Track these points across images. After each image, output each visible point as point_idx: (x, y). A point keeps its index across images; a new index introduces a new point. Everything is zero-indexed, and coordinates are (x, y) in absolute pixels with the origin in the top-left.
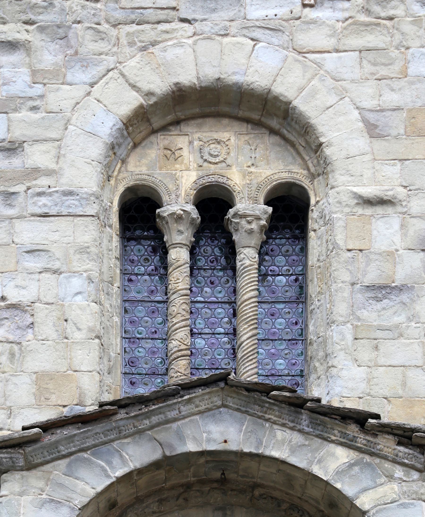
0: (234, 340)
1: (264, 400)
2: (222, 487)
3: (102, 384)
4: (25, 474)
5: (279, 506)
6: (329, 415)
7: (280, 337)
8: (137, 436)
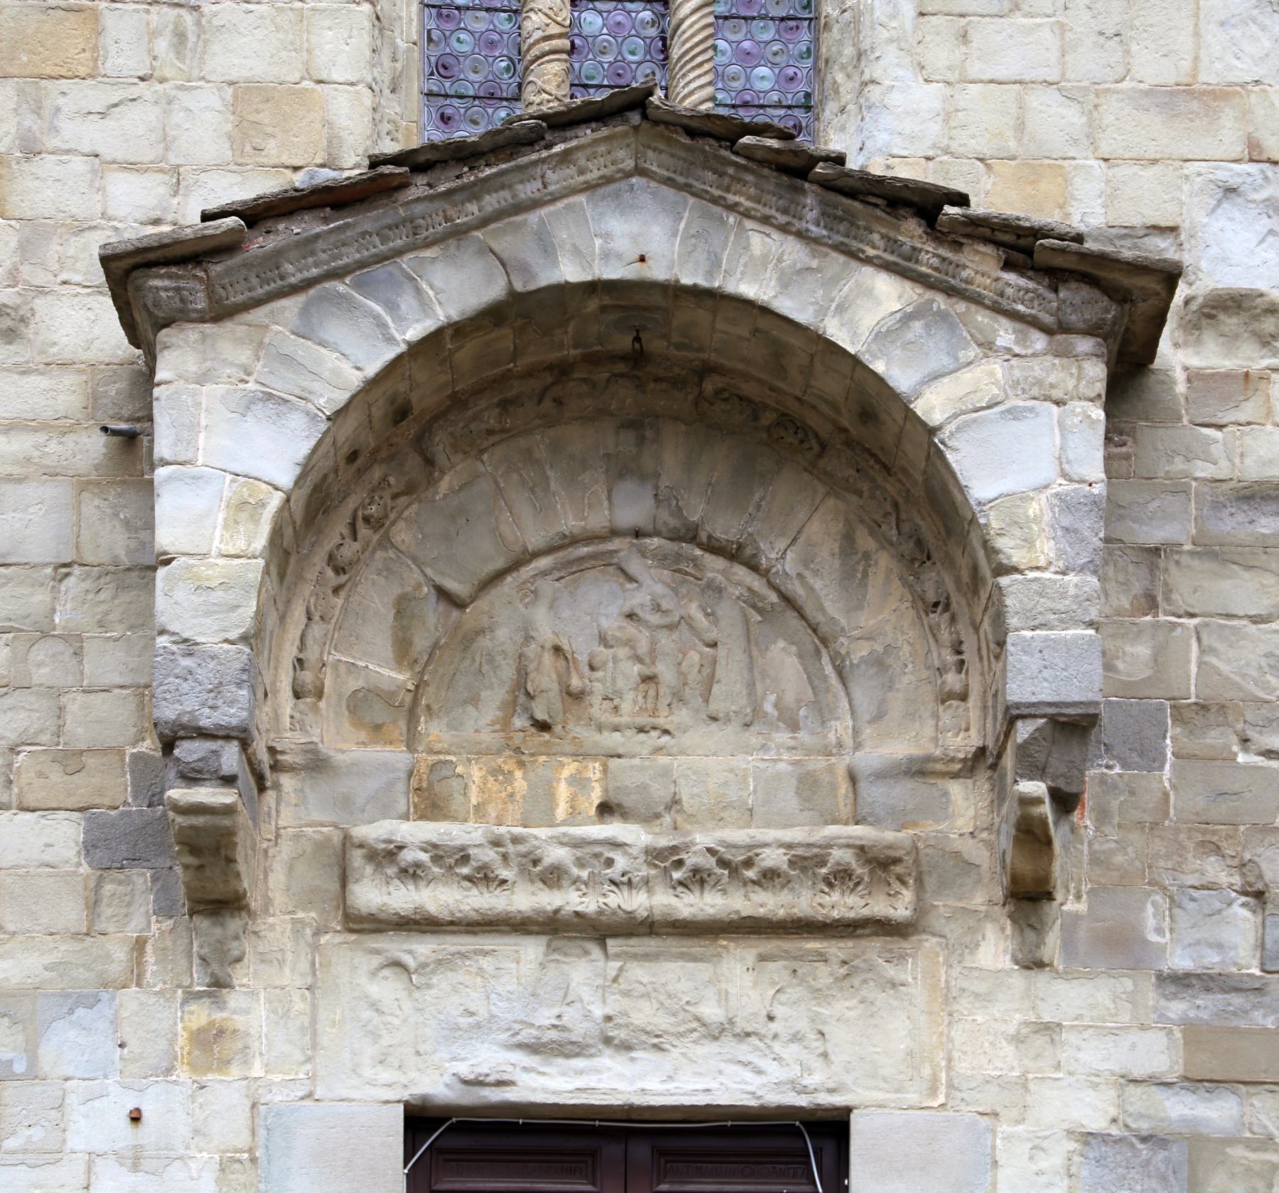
0: (663, 16)
1: (724, 158)
2: (635, 373)
3: (378, 116)
4: (208, 331)
5: (756, 418)
6: (861, 197)
7: (763, 12)
8: (452, 242)
